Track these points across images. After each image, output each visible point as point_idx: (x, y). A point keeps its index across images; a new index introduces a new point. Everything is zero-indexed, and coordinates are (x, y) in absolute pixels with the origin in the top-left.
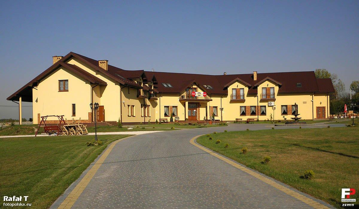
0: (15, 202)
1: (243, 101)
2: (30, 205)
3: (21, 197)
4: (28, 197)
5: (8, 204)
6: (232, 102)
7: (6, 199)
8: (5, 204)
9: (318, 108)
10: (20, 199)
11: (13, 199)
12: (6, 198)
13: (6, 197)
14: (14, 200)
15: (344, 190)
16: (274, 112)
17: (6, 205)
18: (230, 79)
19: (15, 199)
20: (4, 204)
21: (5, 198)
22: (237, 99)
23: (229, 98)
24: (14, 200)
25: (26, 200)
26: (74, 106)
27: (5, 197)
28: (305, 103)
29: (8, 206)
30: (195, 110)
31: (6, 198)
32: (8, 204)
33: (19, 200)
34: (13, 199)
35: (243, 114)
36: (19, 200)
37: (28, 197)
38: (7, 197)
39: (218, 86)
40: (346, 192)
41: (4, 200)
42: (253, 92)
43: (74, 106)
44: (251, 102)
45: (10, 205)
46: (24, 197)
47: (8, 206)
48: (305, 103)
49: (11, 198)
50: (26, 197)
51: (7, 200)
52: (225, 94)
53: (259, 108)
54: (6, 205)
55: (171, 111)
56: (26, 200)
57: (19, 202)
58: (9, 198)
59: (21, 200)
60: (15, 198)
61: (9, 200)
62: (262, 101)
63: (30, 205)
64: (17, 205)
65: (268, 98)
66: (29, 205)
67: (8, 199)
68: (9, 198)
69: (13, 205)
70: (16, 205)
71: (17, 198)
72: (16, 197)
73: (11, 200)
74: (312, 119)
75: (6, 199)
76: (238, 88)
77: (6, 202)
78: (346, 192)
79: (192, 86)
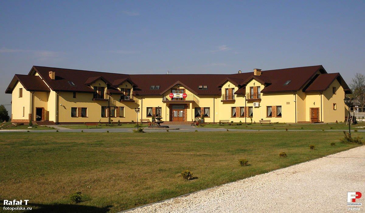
0: (15, 206)
1: (233, 101)
2: (31, 209)
3: (21, 201)
4: (28, 200)
5: (8, 208)
6: (224, 102)
7: (7, 203)
8: (5, 208)
9: (312, 109)
10: (20, 203)
11: (13, 203)
12: (6, 201)
13: (6, 200)
14: (14, 204)
15: (349, 194)
16: (259, 114)
17: (6, 209)
18: (223, 79)
19: (15, 203)
20: (4, 208)
21: (6, 202)
22: (229, 100)
23: (221, 99)
24: (14, 204)
25: (26, 204)
26: (65, 108)
27: (5, 201)
28: (288, 103)
29: (15, 208)
30: (182, 112)
31: (6, 201)
32: (8, 208)
33: (19, 204)
34: (13, 203)
35: (234, 116)
36: (19, 204)
37: (28, 200)
38: (7, 201)
39: (209, 85)
40: (352, 196)
41: (4, 204)
42: (241, 93)
43: (65, 108)
44: (240, 102)
45: (11, 209)
46: (25, 200)
47: (15, 208)
48: (288, 103)
49: (11, 202)
50: (26, 201)
51: (7, 204)
52: (218, 95)
53: (247, 109)
54: (6, 209)
55: (156, 113)
56: (26, 204)
57: (19, 206)
58: (9, 202)
59: (21, 204)
60: (15, 202)
61: (9, 204)
62: (250, 101)
63: (31, 209)
64: (17, 209)
65: (255, 98)
66: (30, 209)
67: (8, 203)
68: (9, 202)
69: (13, 209)
70: (16, 209)
71: (17, 202)
72: (16, 201)
73: (12, 204)
74: (295, 122)
75: (7, 203)
76: (255, 86)
77: (6, 206)
78: (352, 196)
79: (179, 87)
